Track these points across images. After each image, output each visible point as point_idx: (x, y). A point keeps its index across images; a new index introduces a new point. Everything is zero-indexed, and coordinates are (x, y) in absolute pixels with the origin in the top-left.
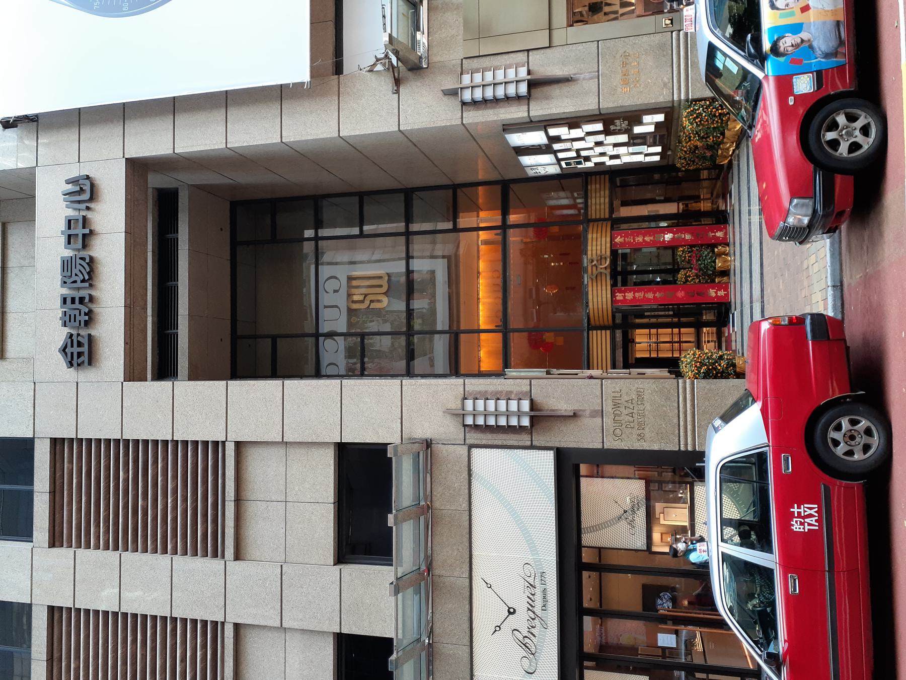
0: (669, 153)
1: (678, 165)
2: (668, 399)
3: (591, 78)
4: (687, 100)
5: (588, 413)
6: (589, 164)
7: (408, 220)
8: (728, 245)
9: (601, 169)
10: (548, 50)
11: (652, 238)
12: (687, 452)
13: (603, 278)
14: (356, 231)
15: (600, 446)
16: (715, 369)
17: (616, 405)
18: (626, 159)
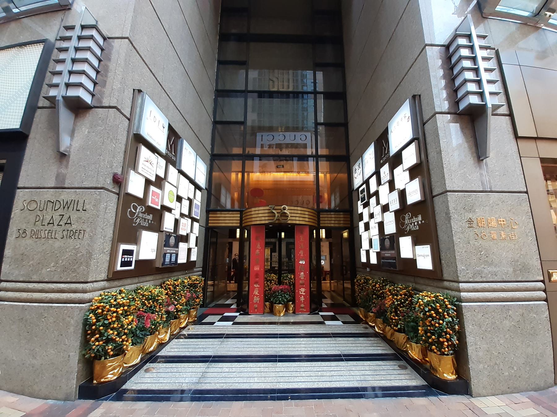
0: (368, 270)
1: (358, 277)
2: (65, 269)
3: (483, 184)
4: (460, 300)
5: (63, 171)
6: (360, 209)
7: (328, 158)
8: (294, 312)
9: (356, 218)
10: (512, 136)
11: (302, 255)
12: (202, 271)
13: (271, 218)
14: (321, 119)
15: (20, 184)
16: (93, 334)
17: (67, 205)
18: (365, 236)
